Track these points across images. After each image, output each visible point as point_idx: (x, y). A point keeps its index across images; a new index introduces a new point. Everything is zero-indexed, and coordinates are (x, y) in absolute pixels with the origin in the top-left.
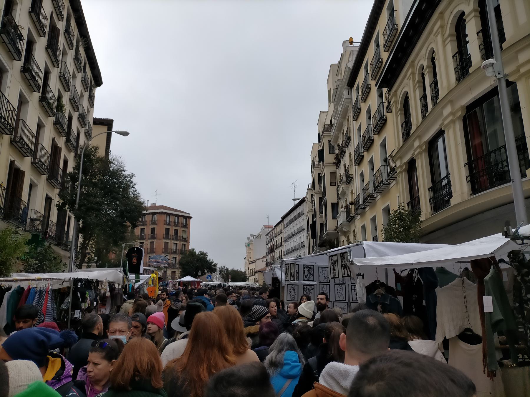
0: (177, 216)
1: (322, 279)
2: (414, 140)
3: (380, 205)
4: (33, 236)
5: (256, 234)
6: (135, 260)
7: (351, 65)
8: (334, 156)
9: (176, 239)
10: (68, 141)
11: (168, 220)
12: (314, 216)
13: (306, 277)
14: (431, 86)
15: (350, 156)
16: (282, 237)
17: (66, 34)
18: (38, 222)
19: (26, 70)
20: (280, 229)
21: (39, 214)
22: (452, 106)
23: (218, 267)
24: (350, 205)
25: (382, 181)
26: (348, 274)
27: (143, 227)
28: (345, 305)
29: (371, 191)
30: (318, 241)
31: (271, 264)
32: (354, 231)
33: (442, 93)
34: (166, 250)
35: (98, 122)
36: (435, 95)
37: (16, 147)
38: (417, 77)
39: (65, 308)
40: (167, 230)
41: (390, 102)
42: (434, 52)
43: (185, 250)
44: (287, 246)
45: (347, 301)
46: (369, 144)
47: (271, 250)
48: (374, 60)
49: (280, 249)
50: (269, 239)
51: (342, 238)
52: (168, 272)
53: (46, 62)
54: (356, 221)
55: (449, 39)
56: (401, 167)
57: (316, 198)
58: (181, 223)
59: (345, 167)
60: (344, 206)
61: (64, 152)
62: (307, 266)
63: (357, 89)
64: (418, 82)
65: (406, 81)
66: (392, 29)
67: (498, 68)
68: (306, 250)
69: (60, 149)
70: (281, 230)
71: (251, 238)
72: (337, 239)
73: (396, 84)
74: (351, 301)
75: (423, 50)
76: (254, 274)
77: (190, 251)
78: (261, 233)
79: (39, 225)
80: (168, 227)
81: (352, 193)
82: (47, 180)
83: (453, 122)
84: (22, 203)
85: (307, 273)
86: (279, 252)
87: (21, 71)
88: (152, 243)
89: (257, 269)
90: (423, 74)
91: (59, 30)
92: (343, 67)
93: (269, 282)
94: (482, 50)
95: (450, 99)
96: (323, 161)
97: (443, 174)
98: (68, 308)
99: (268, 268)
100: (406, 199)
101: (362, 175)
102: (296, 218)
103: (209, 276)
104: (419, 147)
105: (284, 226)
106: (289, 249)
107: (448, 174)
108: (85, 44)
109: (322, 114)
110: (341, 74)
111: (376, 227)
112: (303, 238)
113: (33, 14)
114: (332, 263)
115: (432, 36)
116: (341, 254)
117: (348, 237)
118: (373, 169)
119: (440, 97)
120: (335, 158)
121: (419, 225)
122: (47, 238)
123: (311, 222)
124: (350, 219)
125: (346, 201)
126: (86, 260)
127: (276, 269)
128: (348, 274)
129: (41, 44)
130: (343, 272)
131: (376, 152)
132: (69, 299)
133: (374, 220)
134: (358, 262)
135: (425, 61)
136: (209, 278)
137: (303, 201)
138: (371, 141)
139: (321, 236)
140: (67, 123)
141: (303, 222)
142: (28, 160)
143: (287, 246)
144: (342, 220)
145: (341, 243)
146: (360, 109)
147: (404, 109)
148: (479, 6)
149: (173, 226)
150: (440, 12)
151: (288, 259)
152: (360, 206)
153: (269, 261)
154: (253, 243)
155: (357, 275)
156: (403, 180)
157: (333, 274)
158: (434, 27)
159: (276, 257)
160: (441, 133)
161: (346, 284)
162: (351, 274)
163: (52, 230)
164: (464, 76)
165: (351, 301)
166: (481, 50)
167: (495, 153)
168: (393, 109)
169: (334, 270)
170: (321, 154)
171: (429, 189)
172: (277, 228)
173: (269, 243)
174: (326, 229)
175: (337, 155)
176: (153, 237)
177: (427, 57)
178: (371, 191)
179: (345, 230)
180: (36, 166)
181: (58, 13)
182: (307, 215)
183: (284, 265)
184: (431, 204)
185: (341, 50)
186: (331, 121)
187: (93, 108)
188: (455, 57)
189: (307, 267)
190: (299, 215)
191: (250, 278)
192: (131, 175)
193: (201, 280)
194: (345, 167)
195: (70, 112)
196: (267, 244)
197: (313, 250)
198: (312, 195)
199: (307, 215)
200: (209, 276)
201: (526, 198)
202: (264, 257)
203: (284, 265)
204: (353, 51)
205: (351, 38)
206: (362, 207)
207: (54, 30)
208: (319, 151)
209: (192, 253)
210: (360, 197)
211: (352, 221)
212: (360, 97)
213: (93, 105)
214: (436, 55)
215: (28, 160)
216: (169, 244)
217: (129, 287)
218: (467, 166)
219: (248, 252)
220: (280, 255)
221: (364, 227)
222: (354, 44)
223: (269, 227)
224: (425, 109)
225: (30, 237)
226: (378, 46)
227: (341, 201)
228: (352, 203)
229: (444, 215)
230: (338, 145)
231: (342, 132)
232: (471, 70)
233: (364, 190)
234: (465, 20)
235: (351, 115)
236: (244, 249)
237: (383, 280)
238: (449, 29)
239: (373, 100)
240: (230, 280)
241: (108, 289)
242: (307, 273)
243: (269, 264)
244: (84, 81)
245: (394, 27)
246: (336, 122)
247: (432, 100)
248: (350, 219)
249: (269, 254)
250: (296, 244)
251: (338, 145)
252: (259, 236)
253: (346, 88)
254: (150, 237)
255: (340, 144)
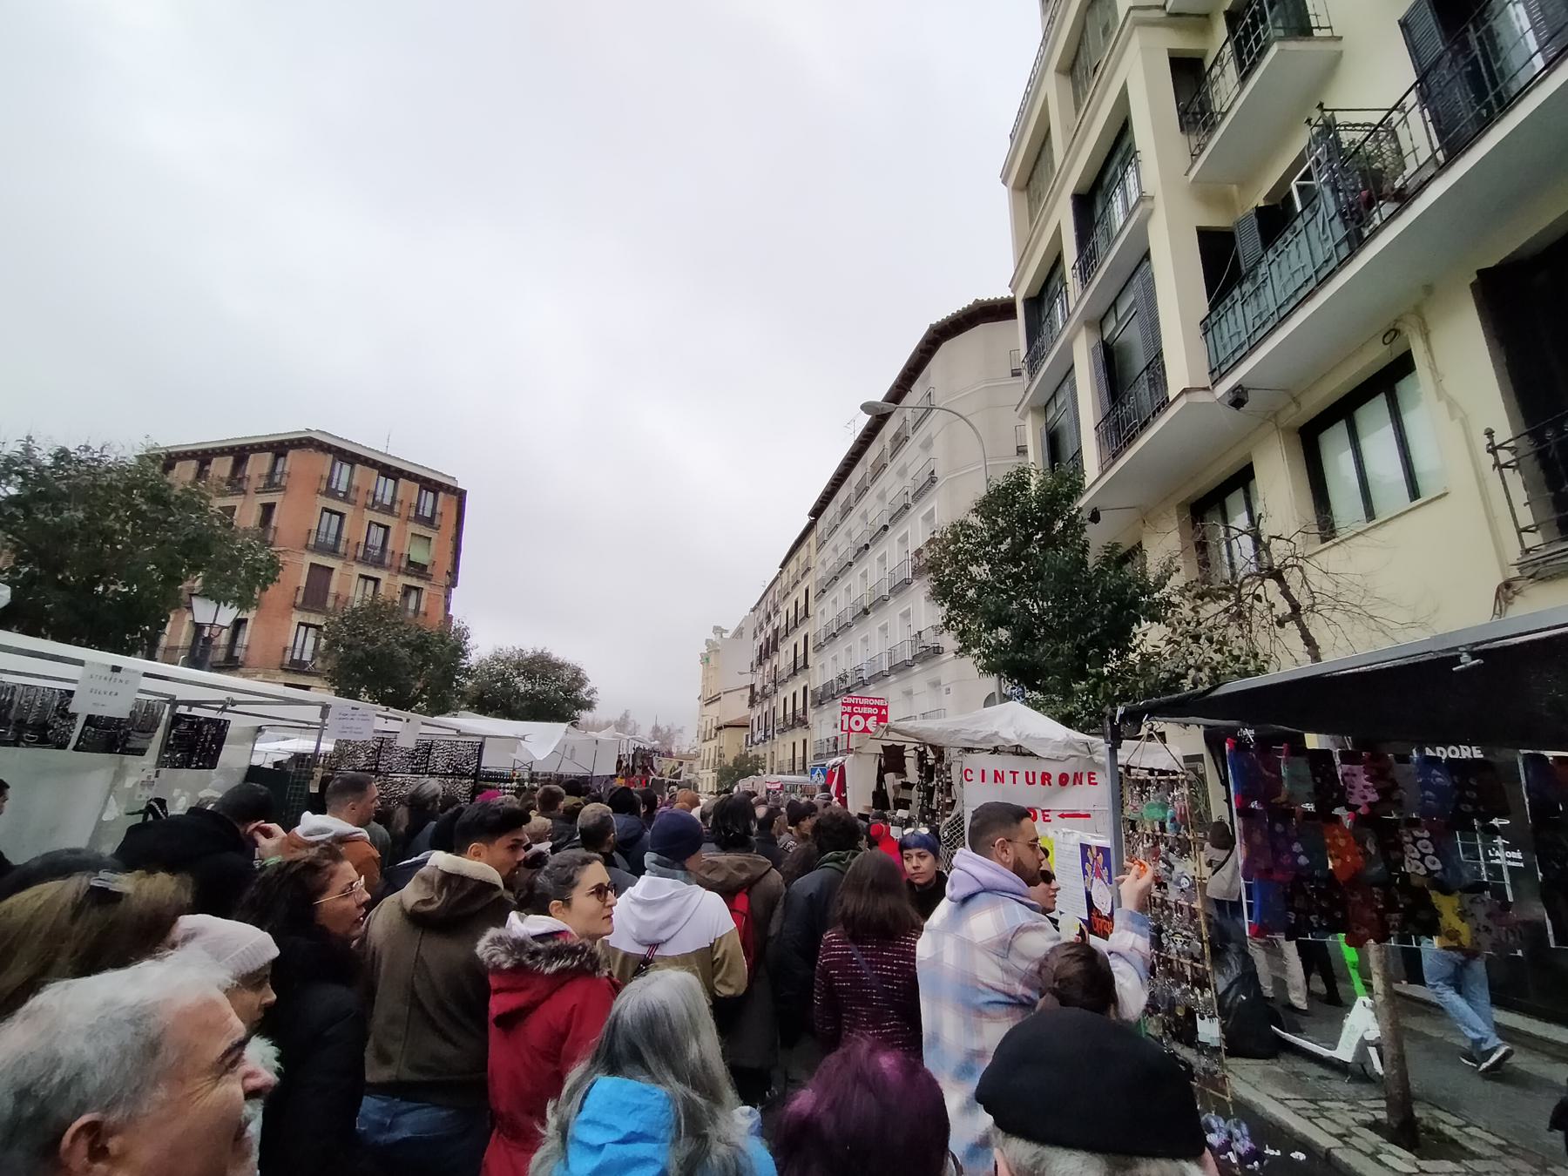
16: (806, 637)
31: (765, 696)
58: (406, 504)
76: (716, 735)
78: (743, 625)
86: (794, 694)
89: (724, 720)
149: (366, 506)
154: (718, 651)
173: (762, 629)
196: (755, 637)
243: (758, 698)
249: (761, 664)
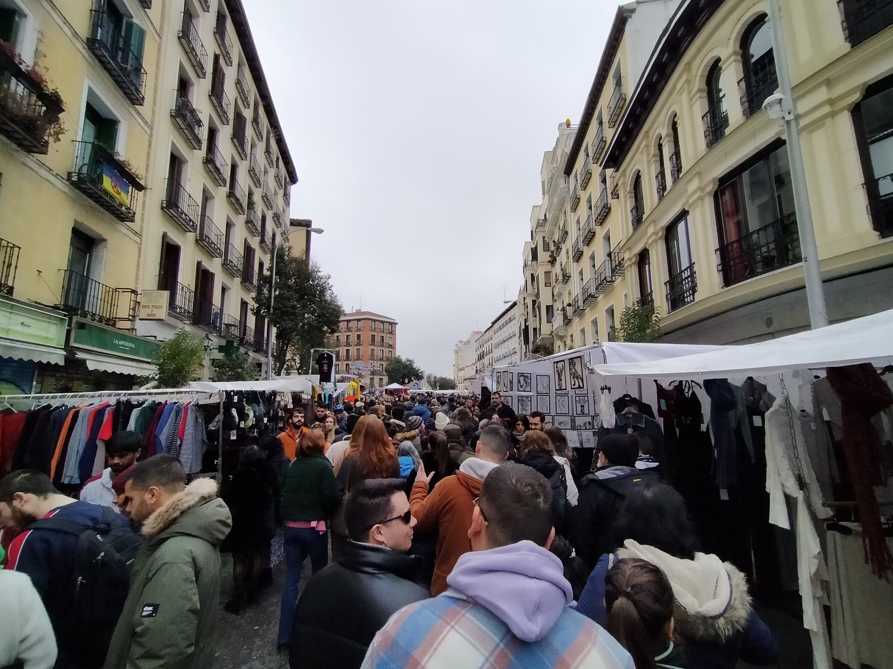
0: (383, 322)
1: (540, 389)
2: (647, 227)
3: (603, 303)
4: (228, 342)
5: (465, 340)
6: (325, 367)
7: (568, 150)
8: (549, 253)
9: (382, 346)
10: (262, 241)
11: (373, 326)
12: (526, 321)
13: (521, 387)
14: (671, 158)
15: (567, 253)
17: (254, 124)
18: (233, 328)
19: (209, 161)
20: (490, 334)
21: (234, 320)
22: (655, 226)
23: (425, 375)
24: (568, 307)
25: (605, 278)
26: (579, 385)
27: (348, 334)
28: (568, 419)
29: (592, 290)
30: (531, 347)
32: (572, 336)
33: (686, 165)
34: (372, 358)
35: (295, 223)
36: (677, 169)
37: (203, 247)
38: (653, 150)
39: (214, 428)
40: (373, 336)
41: (617, 185)
42: (676, 115)
43: (391, 357)
44: (497, 353)
45: (570, 414)
46: (589, 238)
47: (481, 357)
48: (596, 140)
49: (490, 356)
50: (478, 345)
51: (558, 343)
52: (375, 379)
53: (232, 155)
54: (574, 324)
55: (698, 95)
56: (629, 259)
57: (529, 302)
59: (561, 265)
60: (560, 309)
61: (259, 255)
62: (522, 375)
63: (576, 177)
64: (654, 155)
65: (638, 156)
66: (619, 99)
67: (788, 104)
68: (518, 356)
69: (254, 250)
70: (491, 336)
71: (460, 345)
72: (552, 344)
73: (702, 34)
74: (575, 415)
75: (662, 113)
77: (396, 358)
79: (235, 332)
80: (374, 333)
81: (570, 293)
82: (241, 283)
83: (701, 198)
84: (213, 307)
85: (522, 382)
87: (204, 163)
88: (348, 350)
90: (660, 146)
91: (245, 119)
92: (559, 153)
93: (478, 392)
94: (744, 103)
95: (697, 170)
96: (537, 260)
97: (685, 264)
98: (219, 429)
99: (478, 376)
100: (636, 295)
101: (581, 273)
102: (507, 323)
103: (416, 383)
104: (655, 233)
105: (494, 331)
106: (500, 356)
107: (691, 266)
108: (276, 136)
109: (535, 208)
110: (557, 162)
111: (597, 330)
112: (516, 343)
113: (213, 98)
114: (558, 371)
115: (674, 95)
116: (569, 359)
117: (565, 342)
118: (594, 266)
119: (684, 170)
120: (550, 256)
121: (657, 323)
122: (244, 345)
123: (523, 327)
124: (567, 321)
125: (563, 303)
126: (285, 366)
127: (485, 378)
128: (579, 385)
129: (225, 134)
130: (573, 383)
131: (599, 247)
132: (220, 417)
133: (595, 322)
134: (600, 369)
135: (664, 128)
136: (416, 385)
137: (515, 304)
138: (580, 253)
139: (533, 342)
140: (260, 222)
141: (515, 327)
142: (218, 261)
143: (497, 353)
144: (558, 322)
145: (556, 349)
146: (579, 199)
147: (706, 88)
148: (741, 48)
150: (686, 62)
151: (501, 366)
152: (578, 307)
153: (478, 368)
155: (602, 389)
156: (632, 274)
157: (559, 385)
158: (677, 84)
159: (485, 364)
160: (683, 215)
161: (569, 395)
162: (583, 385)
163: (250, 336)
164: (717, 140)
165: (575, 415)
166: (742, 104)
167: (759, 234)
168: (621, 193)
169: (560, 380)
170: (534, 252)
171: (665, 284)
172: (487, 333)
174: (540, 334)
175: (552, 252)
176: (359, 344)
177: (666, 124)
178: (592, 290)
179: (562, 335)
180: (226, 266)
181: (244, 99)
182: (519, 319)
183: (495, 373)
184: (667, 301)
185: (557, 134)
186: (545, 215)
187: (289, 207)
188: (705, 118)
189: (523, 376)
190: (510, 320)
191: (459, 385)
192: (328, 276)
193: (408, 388)
194: (561, 265)
195: (263, 211)
197: (526, 356)
198: (524, 298)
199: (519, 319)
200: (416, 383)
201: (824, 282)
202: (474, 364)
203: (495, 373)
204: (571, 133)
205: (568, 120)
206: (581, 308)
207: (239, 118)
208: (532, 249)
209: (398, 361)
210: (579, 298)
211: (569, 325)
212: (579, 185)
213: (289, 204)
214: (678, 118)
215: (218, 261)
216: (375, 351)
217: (325, 396)
218: (718, 252)
219: (457, 359)
220: (491, 361)
221: (583, 331)
222: (571, 126)
223: (478, 332)
224: (662, 188)
225: (223, 343)
226: (601, 123)
227: (557, 302)
228: (569, 305)
229: (684, 314)
230: (554, 241)
231: (558, 226)
232: (727, 131)
233: (584, 290)
234: (721, 68)
235: (568, 206)
236: (453, 356)
237: (635, 395)
238: (698, 83)
239: (595, 186)
240: (438, 388)
241: (291, 401)
242: (522, 382)
244: (277, 177)
245: (622, 98)
246: (551, 216)
247: (673, 175)
248: (567, 321)
250: (507, 350)
251: (554, 241)
252: (468, 342)
253: (563, 176)
254: (356, 344)
255: (556, 241)
